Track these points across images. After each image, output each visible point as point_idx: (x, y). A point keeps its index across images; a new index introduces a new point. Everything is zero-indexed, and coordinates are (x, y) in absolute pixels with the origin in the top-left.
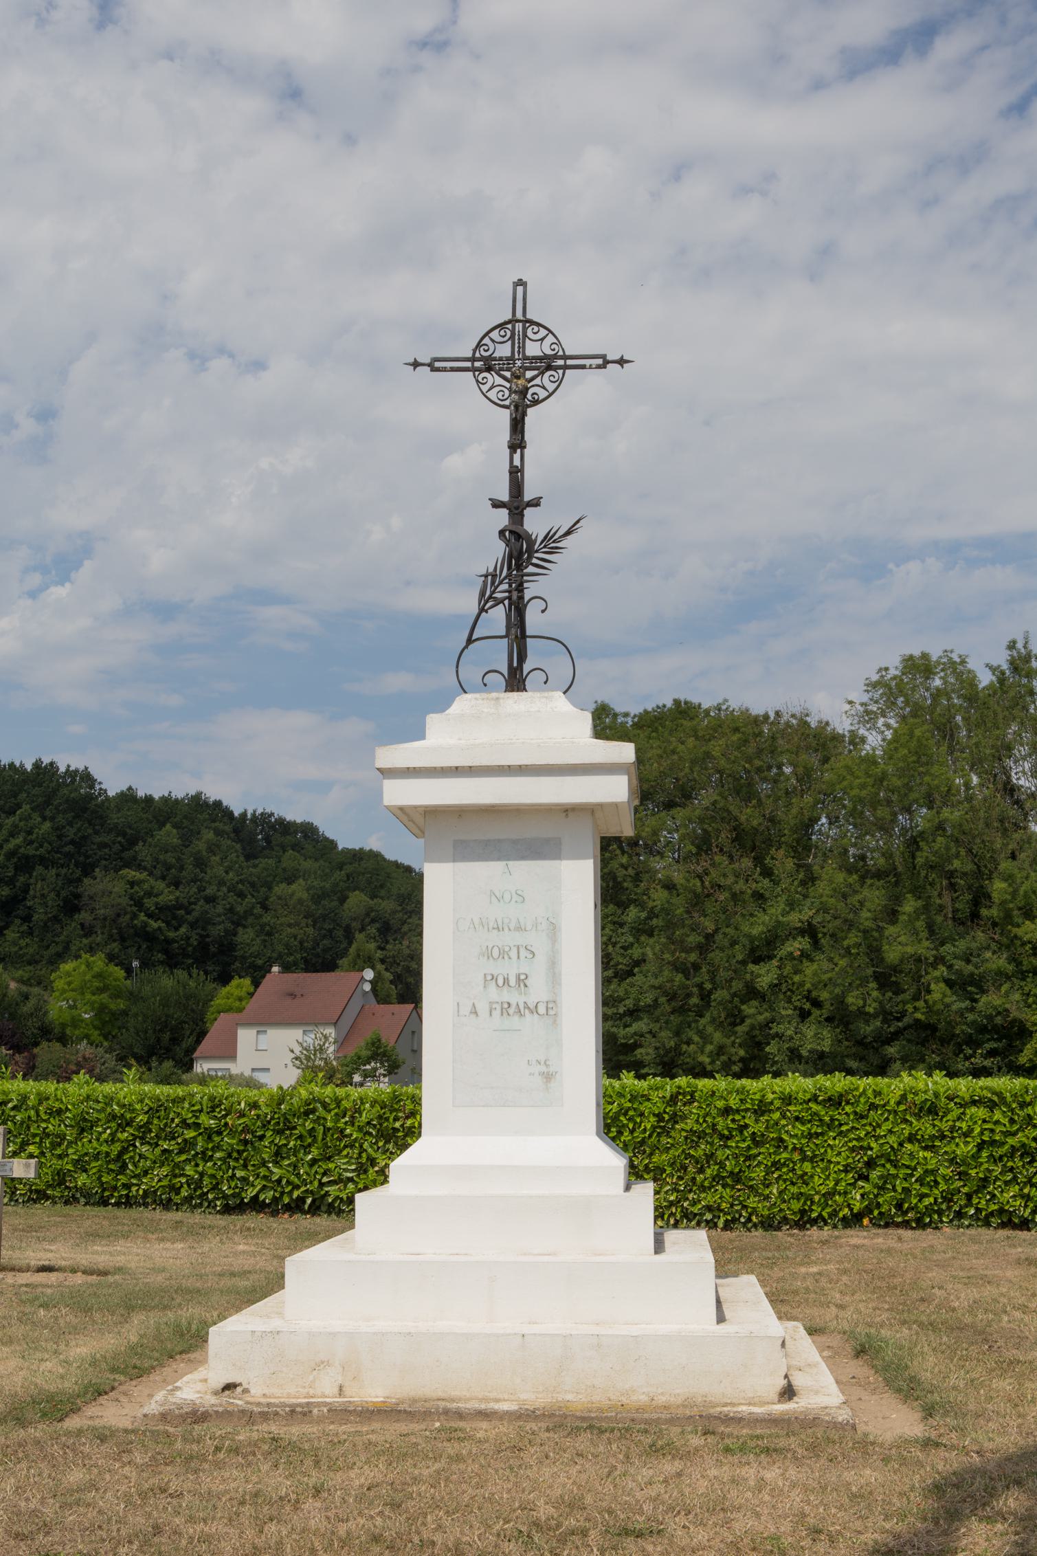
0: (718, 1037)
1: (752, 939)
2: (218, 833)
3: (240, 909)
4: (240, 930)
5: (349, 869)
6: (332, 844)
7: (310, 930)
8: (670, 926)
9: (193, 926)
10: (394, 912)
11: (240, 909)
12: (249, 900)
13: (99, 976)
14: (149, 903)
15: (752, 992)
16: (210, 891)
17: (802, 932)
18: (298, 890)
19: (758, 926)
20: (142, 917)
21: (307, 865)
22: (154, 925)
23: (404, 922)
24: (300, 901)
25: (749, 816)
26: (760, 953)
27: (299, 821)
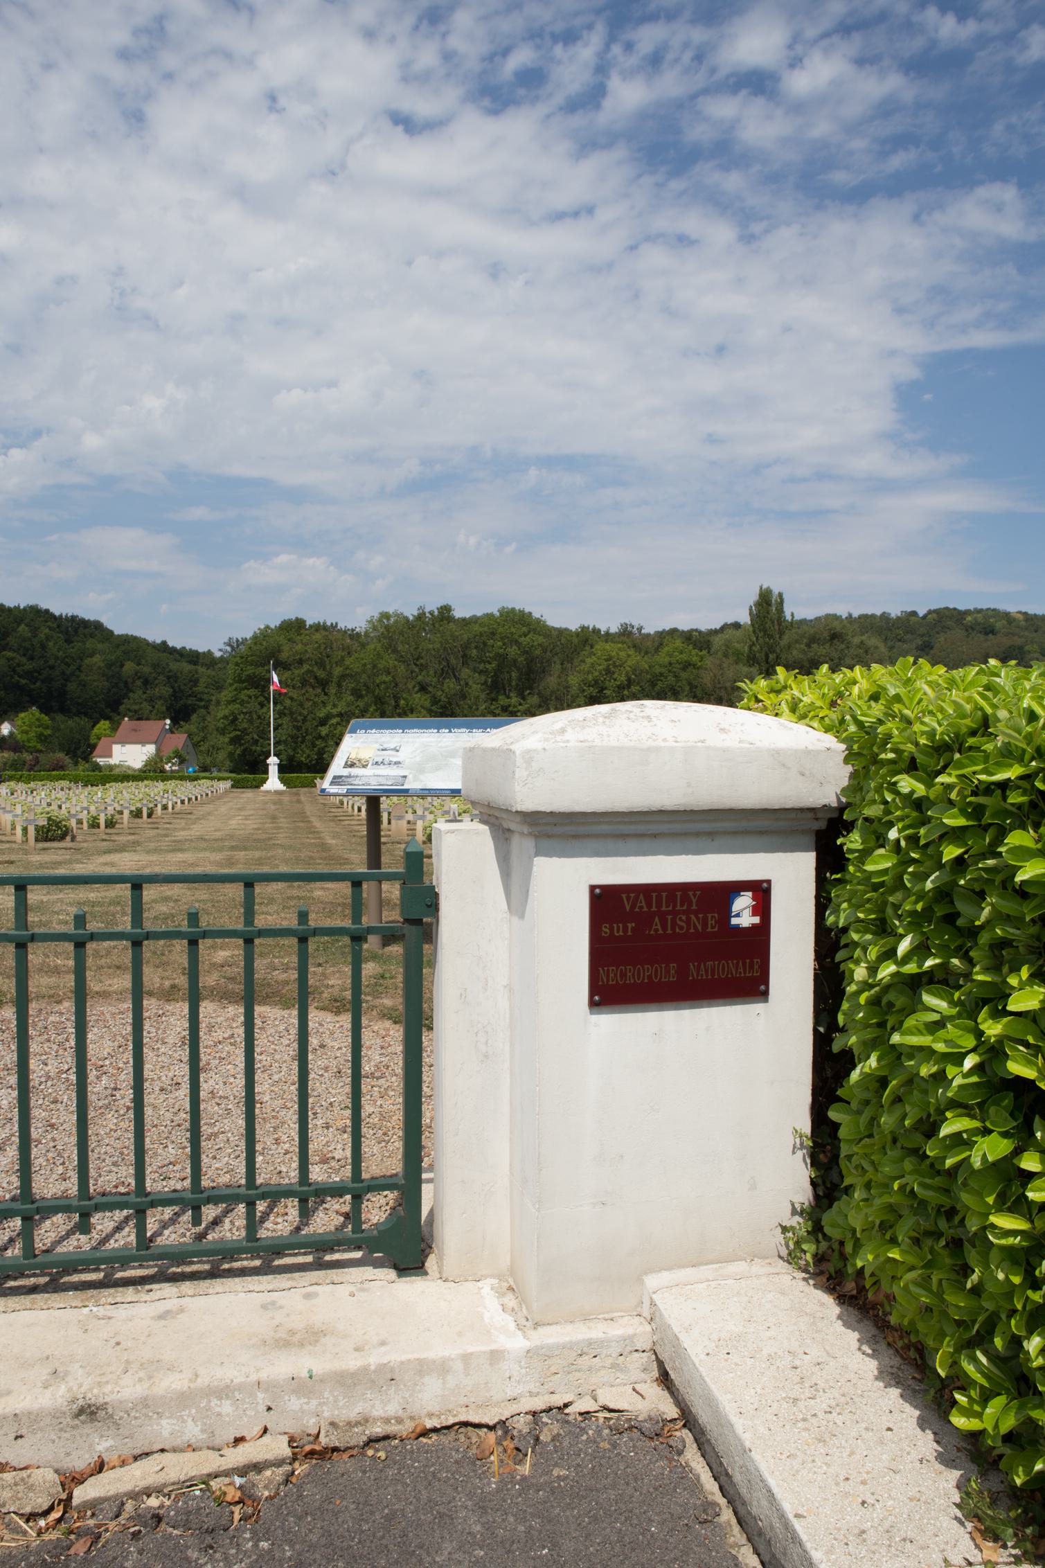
0: (307, 751)
1: (320, 718)
2: (50, 628)
3: (68, 672)
4: (69, 684)
5: (122, 648)
6: (112, 632)
7: (105, 683)
8: (292, 713)
9: (43, 682)
10: (151, 673)
11: (68, 672)
12: (72, 667)
13: (38, 720)
14: (19, 670)
15: (320, 737)
16: (51, 662)
17: (338, 716)
18: (97, 659)
19: (321, 714)
20: (16, 678)
21: (100, 646)
22: (24, 681)
23: (156, 679)
24: (100, 668)
25: (321, 674)
26: (323, 722)
27: (92, 619)
